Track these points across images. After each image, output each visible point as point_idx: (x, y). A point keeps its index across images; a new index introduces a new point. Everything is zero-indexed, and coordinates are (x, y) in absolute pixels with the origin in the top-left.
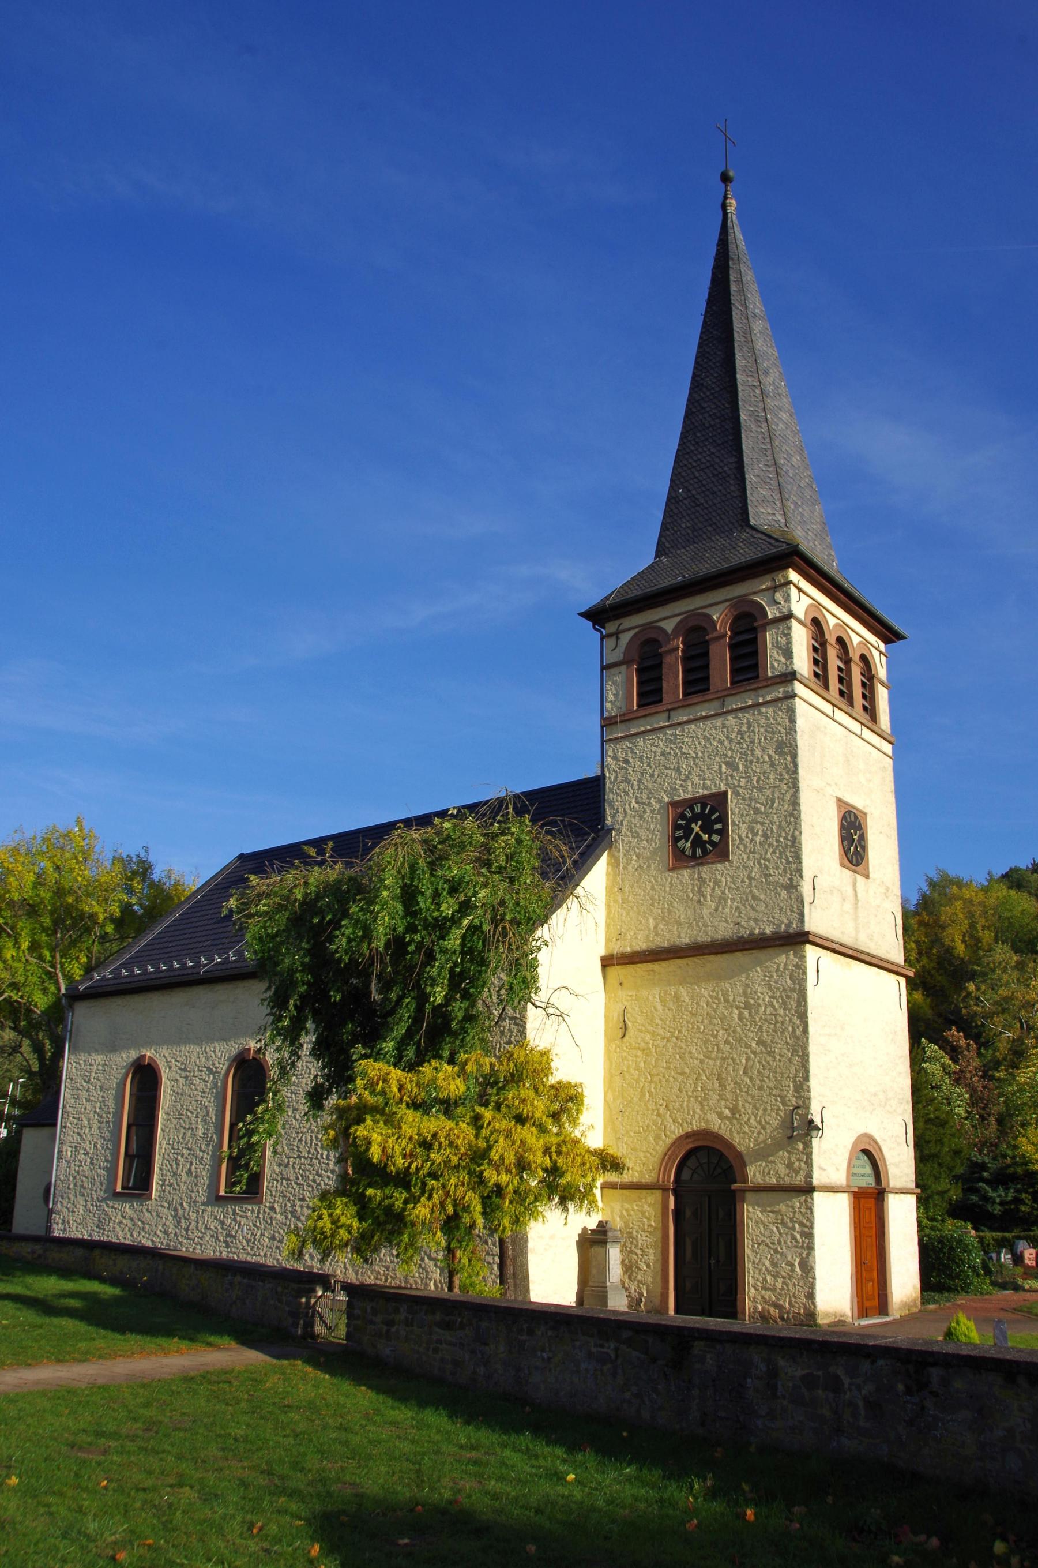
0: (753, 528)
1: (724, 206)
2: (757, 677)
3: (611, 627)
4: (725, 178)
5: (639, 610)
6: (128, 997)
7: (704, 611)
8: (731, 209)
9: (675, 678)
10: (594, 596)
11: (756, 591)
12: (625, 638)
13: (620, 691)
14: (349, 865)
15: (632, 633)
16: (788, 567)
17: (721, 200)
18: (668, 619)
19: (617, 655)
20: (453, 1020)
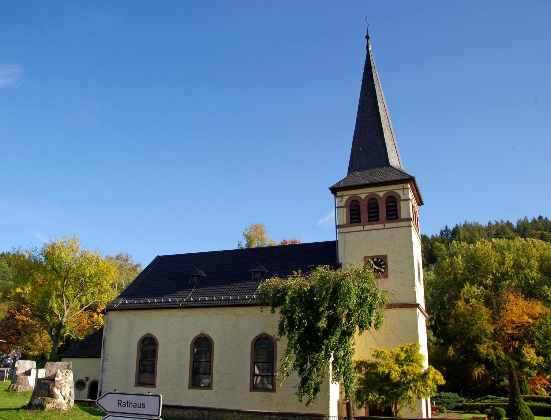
0: (391, 167)
1: (367, 47)
2: (397, 218)
3: (339, 194)
4: (367, 37)
5: (351, 189)
6: (138, 311)
7: (378, 193)
8: (370, 49)
9: (364, 216)
10: (333, 184)
11: (396, 189)
12: (345, 198)
13: (344, 217)
14: (460, 299)
15: (348, 197)
16: (408, 183)
17: (366, 45)
18: (363, 194)
19: (343, 204)
20: (477, 340)
